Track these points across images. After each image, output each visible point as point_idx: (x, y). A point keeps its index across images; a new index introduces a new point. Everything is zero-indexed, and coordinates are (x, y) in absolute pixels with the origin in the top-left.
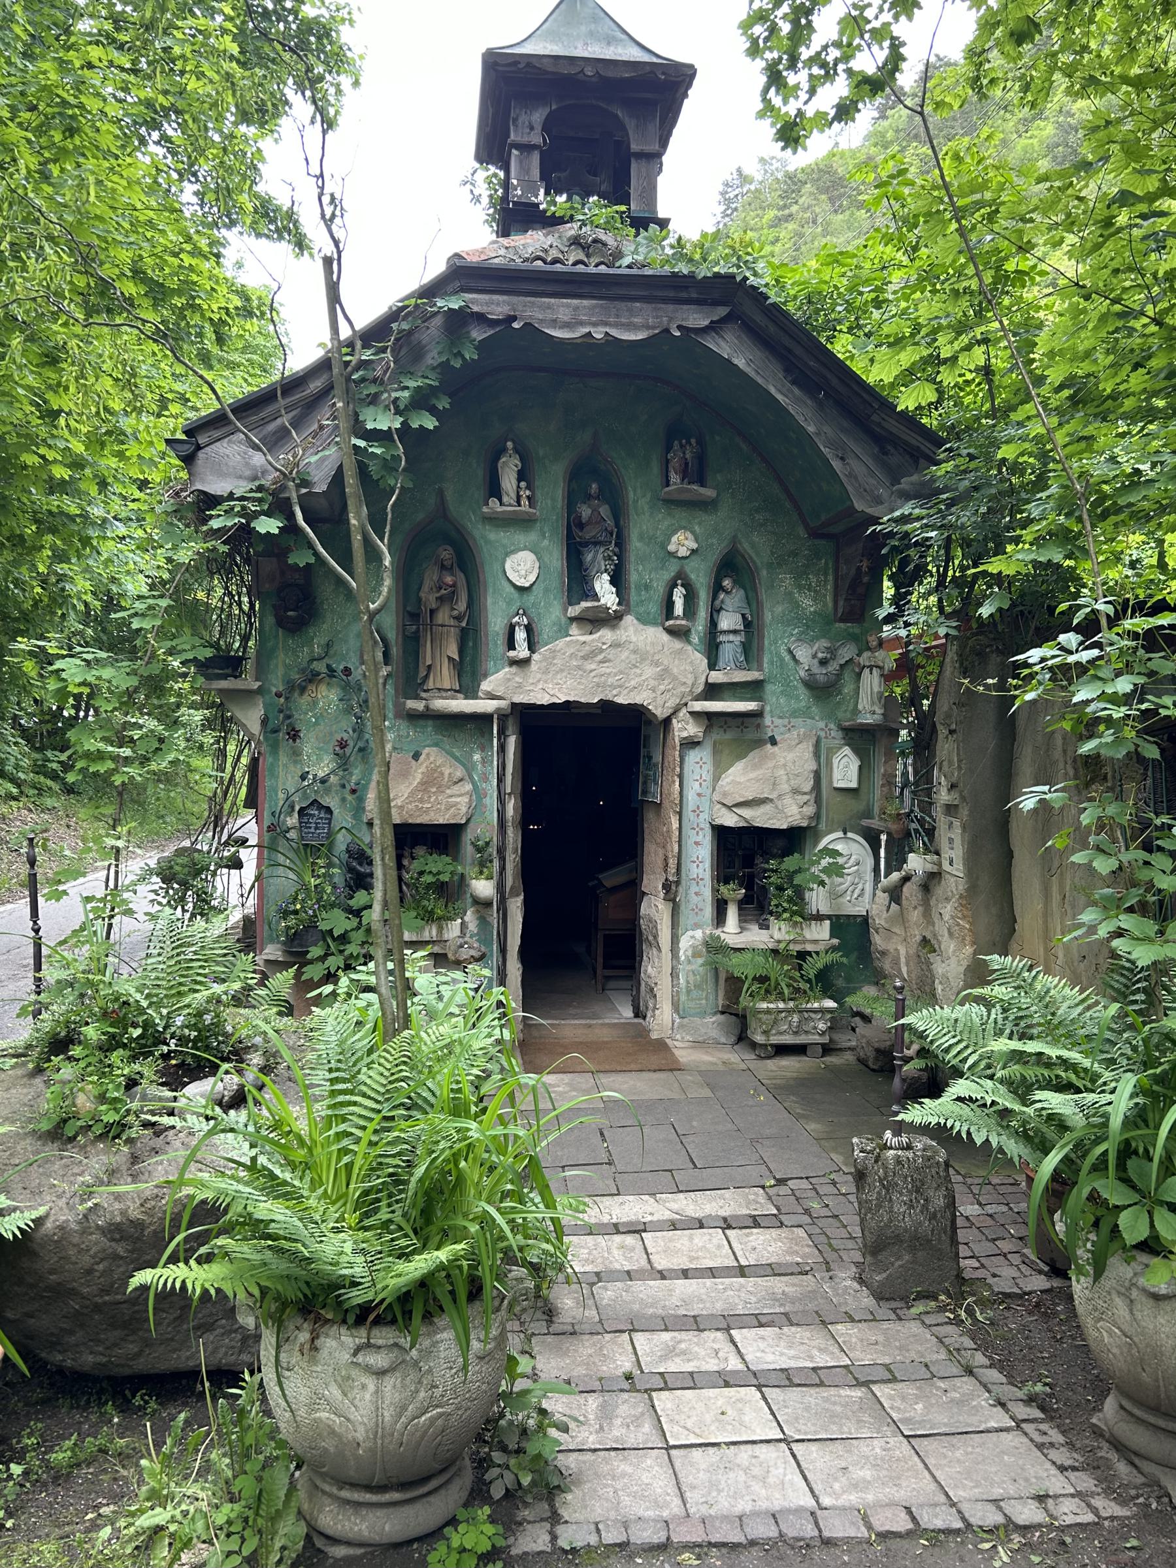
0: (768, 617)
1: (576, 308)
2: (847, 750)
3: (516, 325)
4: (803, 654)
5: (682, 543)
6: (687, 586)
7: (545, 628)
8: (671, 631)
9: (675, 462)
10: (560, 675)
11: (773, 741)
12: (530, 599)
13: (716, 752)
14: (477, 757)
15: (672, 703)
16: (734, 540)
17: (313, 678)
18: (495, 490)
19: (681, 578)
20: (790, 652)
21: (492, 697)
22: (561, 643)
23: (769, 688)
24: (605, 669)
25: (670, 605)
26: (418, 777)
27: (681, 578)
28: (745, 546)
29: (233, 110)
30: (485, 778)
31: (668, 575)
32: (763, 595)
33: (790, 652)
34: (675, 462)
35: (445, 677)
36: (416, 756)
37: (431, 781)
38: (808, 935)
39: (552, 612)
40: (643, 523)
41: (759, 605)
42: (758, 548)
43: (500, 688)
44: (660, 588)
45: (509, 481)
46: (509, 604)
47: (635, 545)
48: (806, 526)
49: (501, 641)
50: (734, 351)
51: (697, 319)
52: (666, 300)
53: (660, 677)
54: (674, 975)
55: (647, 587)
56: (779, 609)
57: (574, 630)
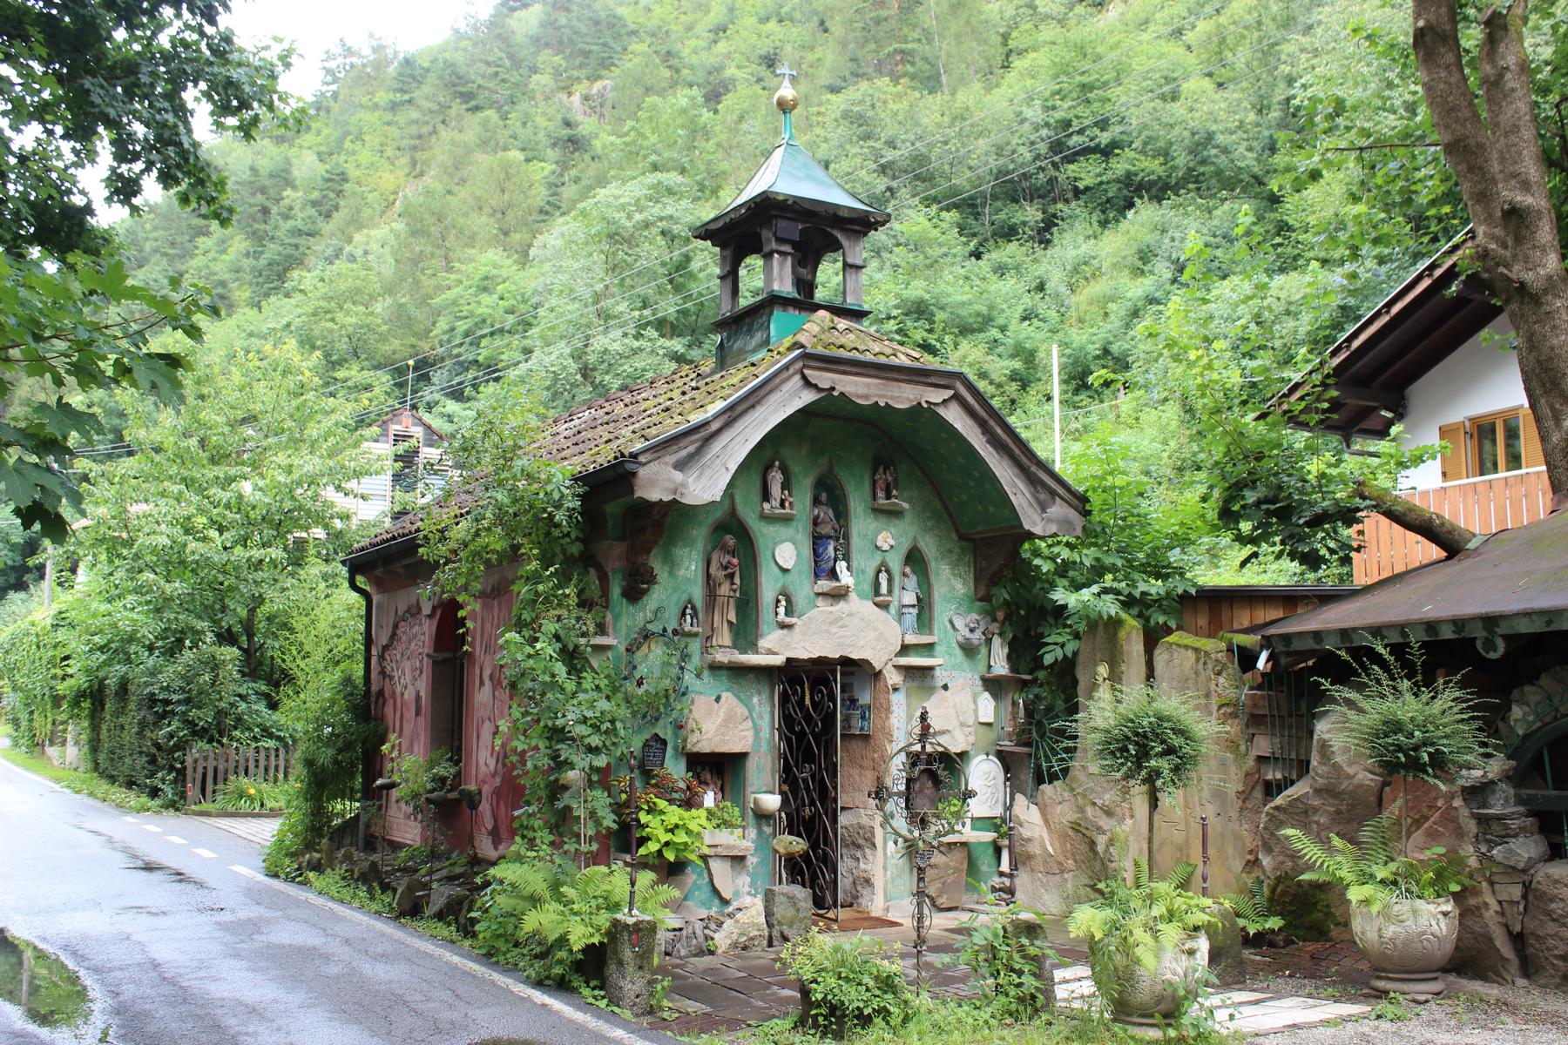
0: (936, 596)
1: (868, 385)
2: (987, 694)
3: (835, 394)
4: (959, 623)
5: (885, 539)
6: (888, 571)
7: (800, 599)
8: (876, 604)
9: (881, 483)
10: (813, 635)
11: (945, 687)
12: (789, 578)
13: (908, 696)
14: (755, 700)
15: (884, 659)
16: (915, 539)
17: (647, 636)
18: (766, 496)
19: (883, 567)
20: (951, 622)
21: (770, 652)
22: (814, 612)
23: (938, 648)
24: (842, 632)
26: (722, 715)
27: (883, 567)
28: (922, 545)
29: (1300, 439)
30: (761, 717)
31: (875, 563)
32: (933, 581)
33: (951, 622)
34: (881, 483)
35: (725, 637)
36: (718, 699)
37: (729, 720)
38: (409, 695)
39: (803, 588)
40: (862, 524)
41: (929, 585)
42: (929, 547)
43: (774, 648)
44: (871, 573)
45: (776, 490)
46: (776, 581)
47: (856, 541)
49: (771, 610)
50: (955, 417)
51: (936, 396)
52: (917, 383)
53: (878, 639)
54: (885, 868)
55: (863, 572)
56: (943, 590)
57: (820, 601)
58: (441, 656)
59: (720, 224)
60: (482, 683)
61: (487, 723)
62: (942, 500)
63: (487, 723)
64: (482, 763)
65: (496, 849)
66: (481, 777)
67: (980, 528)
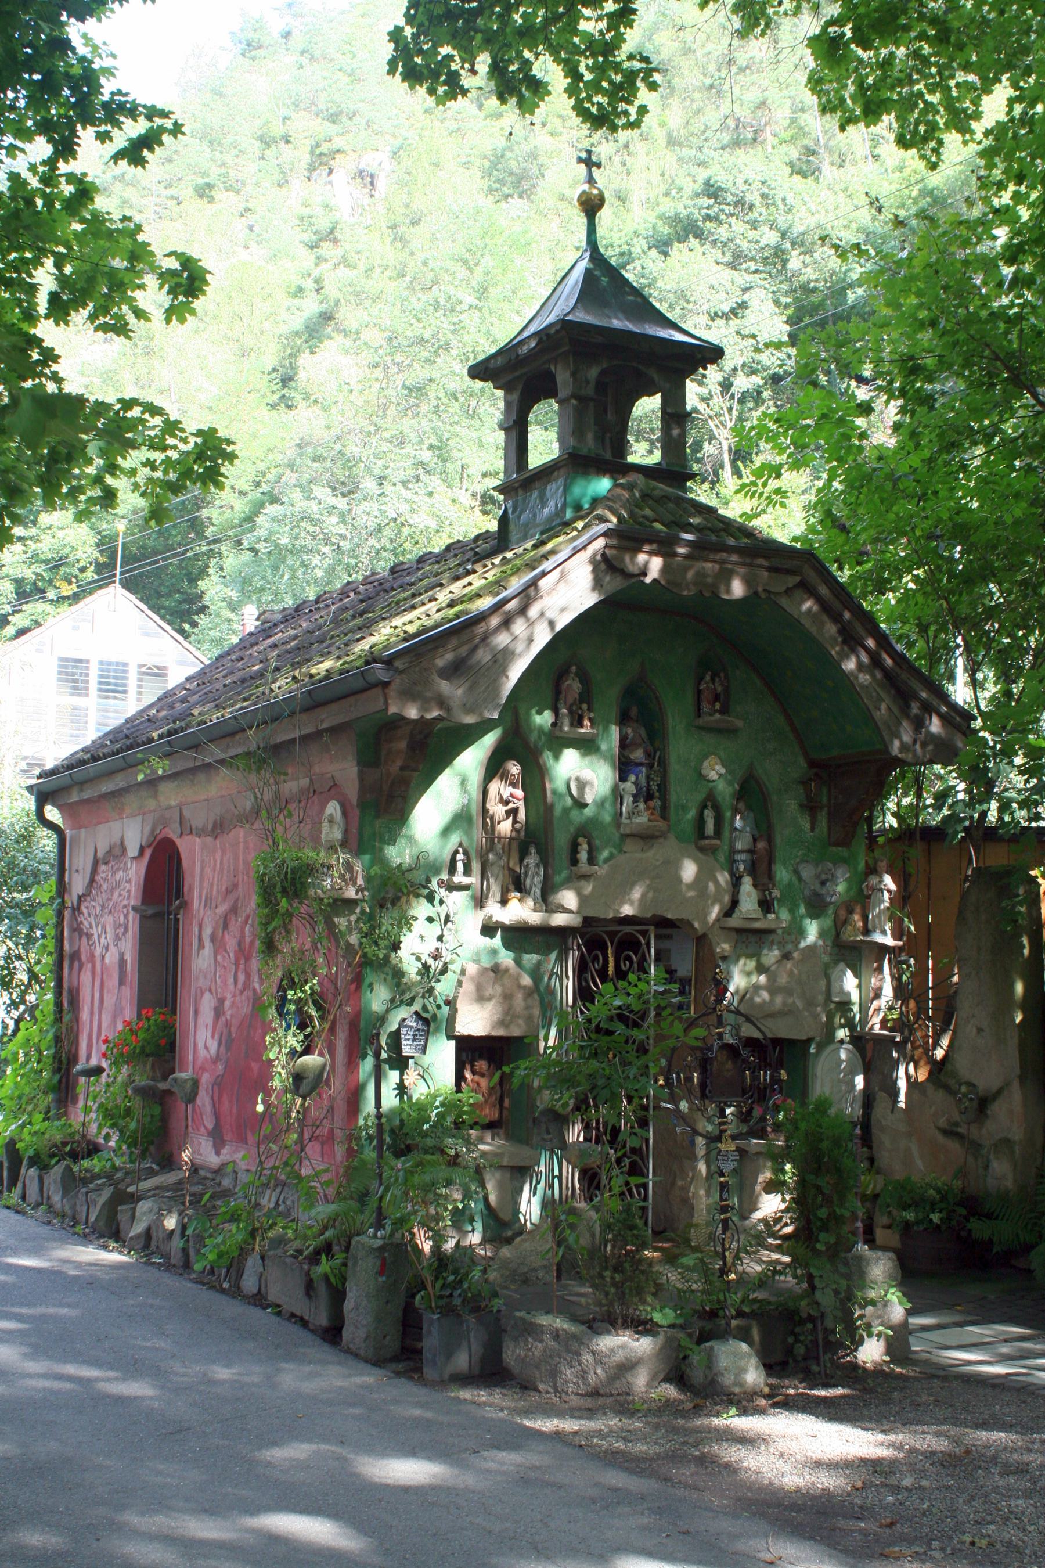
25: (700, 821)
31: (700, 797)
48: (806, 755)
58: (150, 912)
59: (500, 360)
60: (201, 946)
61: (207, 996)
62: (787, 716)
63: (207, 996)
64: (201, 1045)
65: (218, 1153)
66: (199, 1063)
67: (834, 753)
